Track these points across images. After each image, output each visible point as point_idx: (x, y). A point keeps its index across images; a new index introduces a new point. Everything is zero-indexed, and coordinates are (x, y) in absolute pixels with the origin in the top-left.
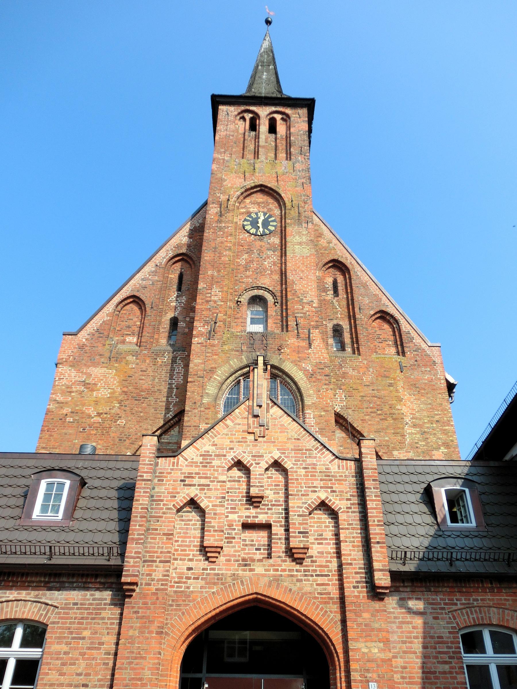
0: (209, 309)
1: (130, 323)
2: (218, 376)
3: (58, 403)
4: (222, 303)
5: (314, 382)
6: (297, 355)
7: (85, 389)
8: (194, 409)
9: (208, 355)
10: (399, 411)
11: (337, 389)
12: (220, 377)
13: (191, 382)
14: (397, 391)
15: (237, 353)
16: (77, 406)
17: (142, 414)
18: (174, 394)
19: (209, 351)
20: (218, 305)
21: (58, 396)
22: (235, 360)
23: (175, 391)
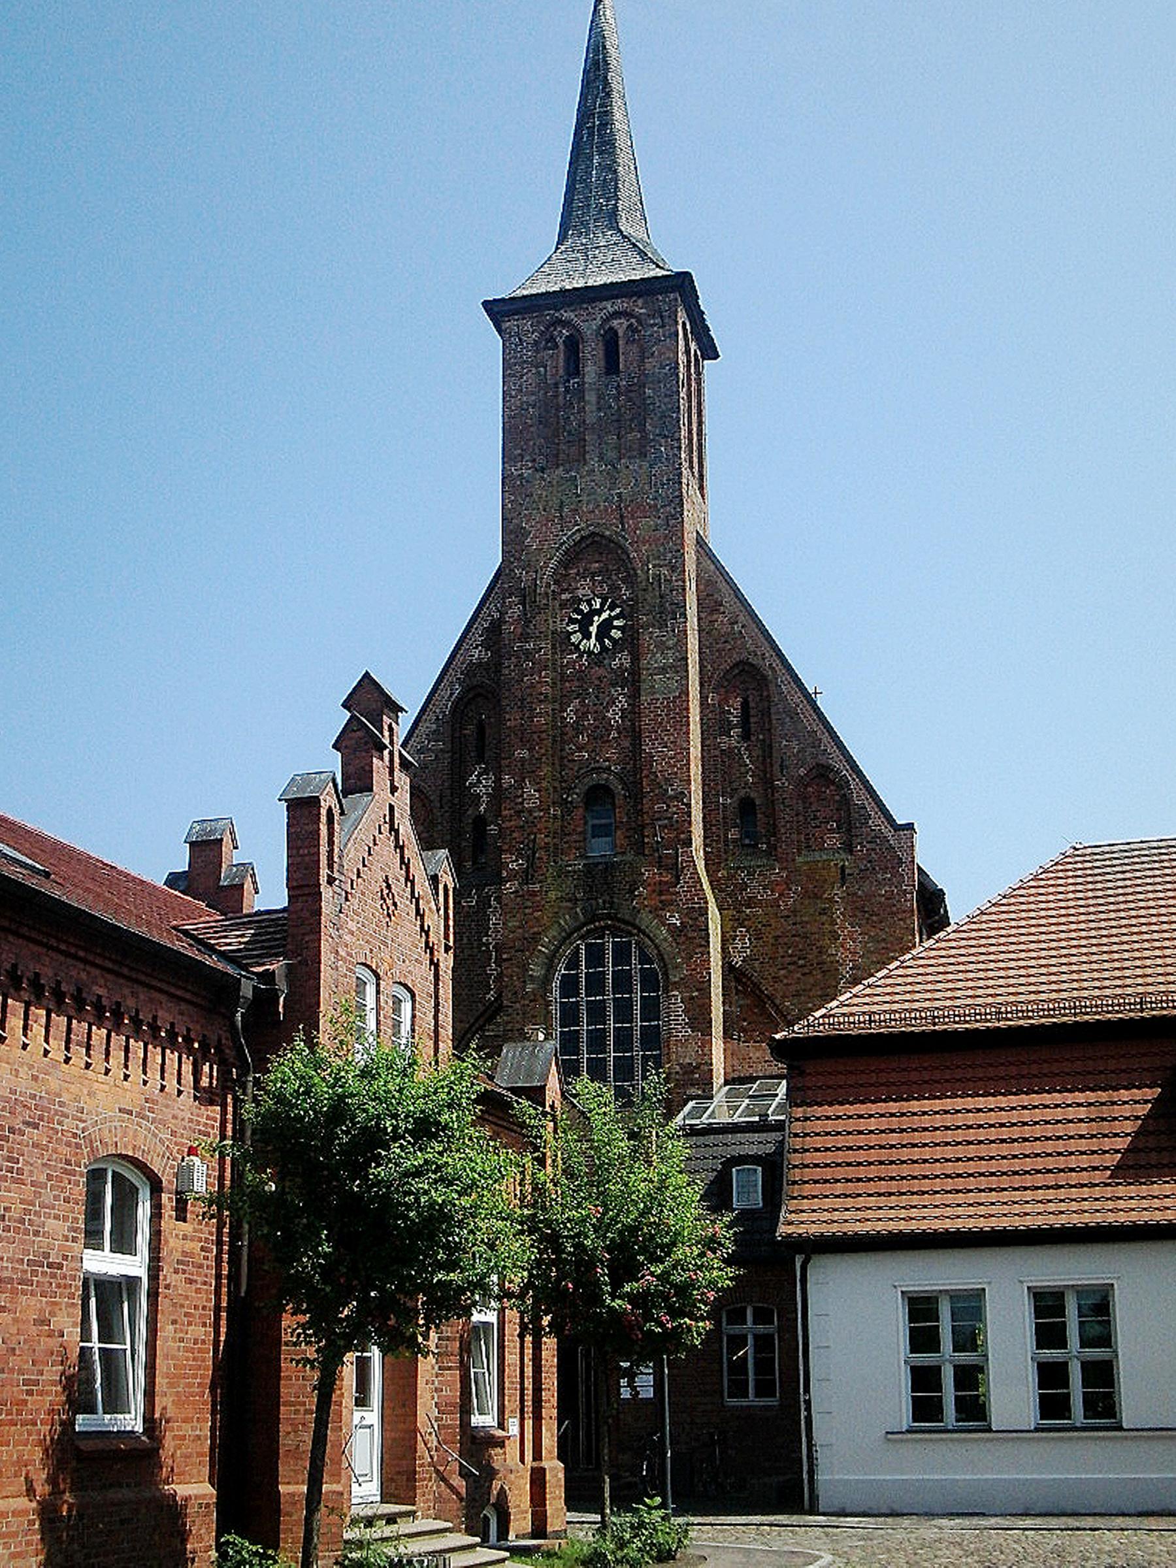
2: (543, 946)
6: (658, 898)
9: (527, 911)
10: (832, 958)
11: (738, 927)
14: (833, 923)
15: (568, 904)
19: (529, 904)
20: (535, 818)
22: (567, 917)
23: (494, 957)
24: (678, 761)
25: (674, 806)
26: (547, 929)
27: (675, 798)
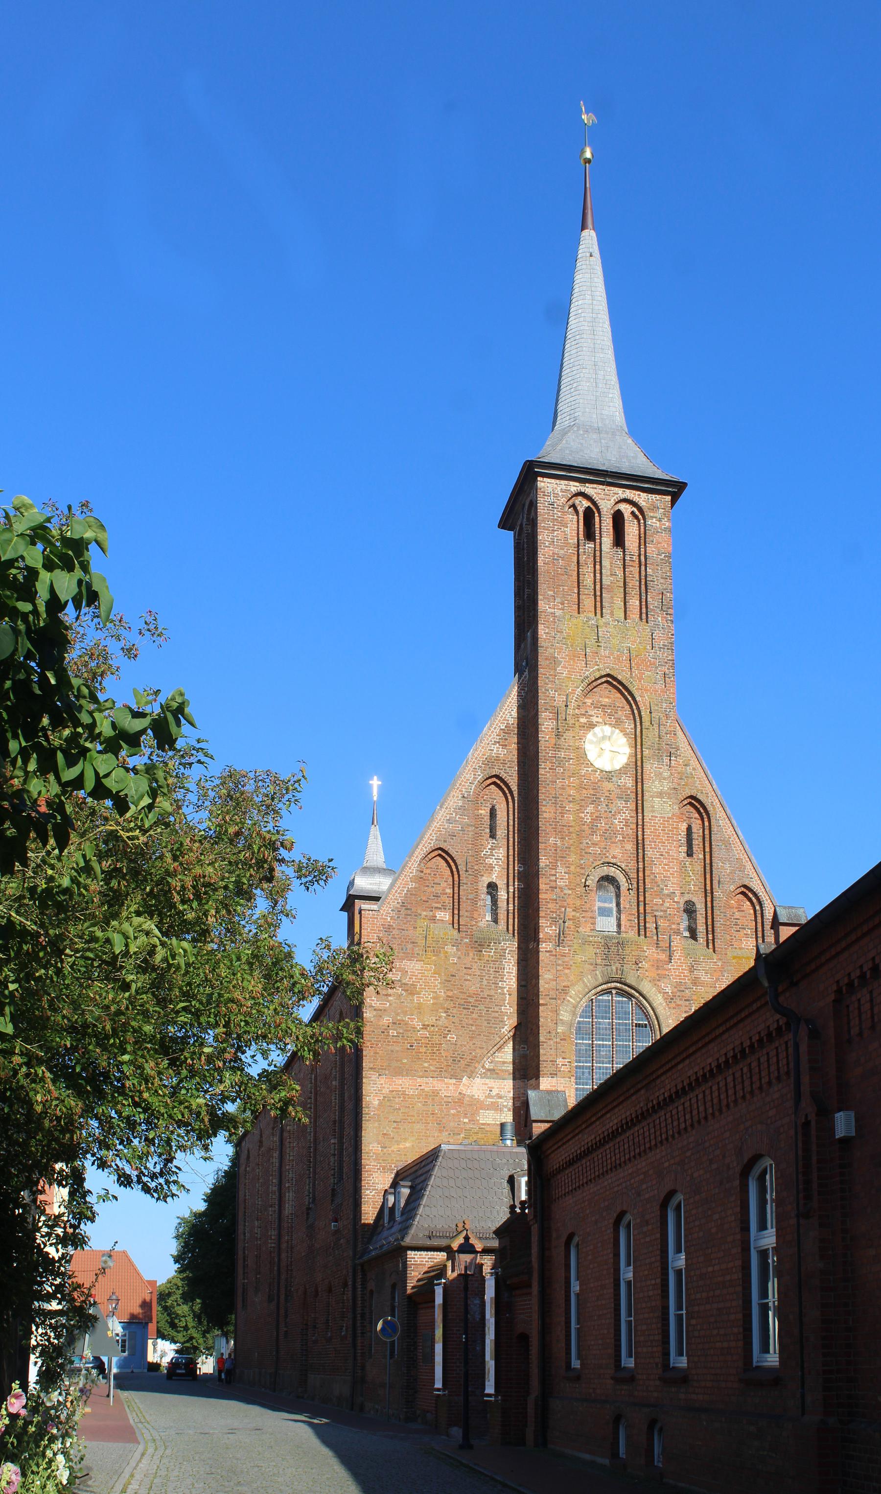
0: (556, 900)
1: (438, 889)
2: (571, 997)
3: (375, 1010)
4: (570, 892)
5: (674, 1008)
7: (403, 992)
8: (550, 1039)
9: (559, 968)
12: (574, 1000)
13: (543, 1005)
16: (398, 1014)
17: (474, 1028)
18: (507, 1002)
19: (560, 962)
20: (565, 894)
21: (374, 1000)
22: (589, 977)
24: (671, 868)
25: (668, 902)
26: (573, 985)
27: (668, 895)
